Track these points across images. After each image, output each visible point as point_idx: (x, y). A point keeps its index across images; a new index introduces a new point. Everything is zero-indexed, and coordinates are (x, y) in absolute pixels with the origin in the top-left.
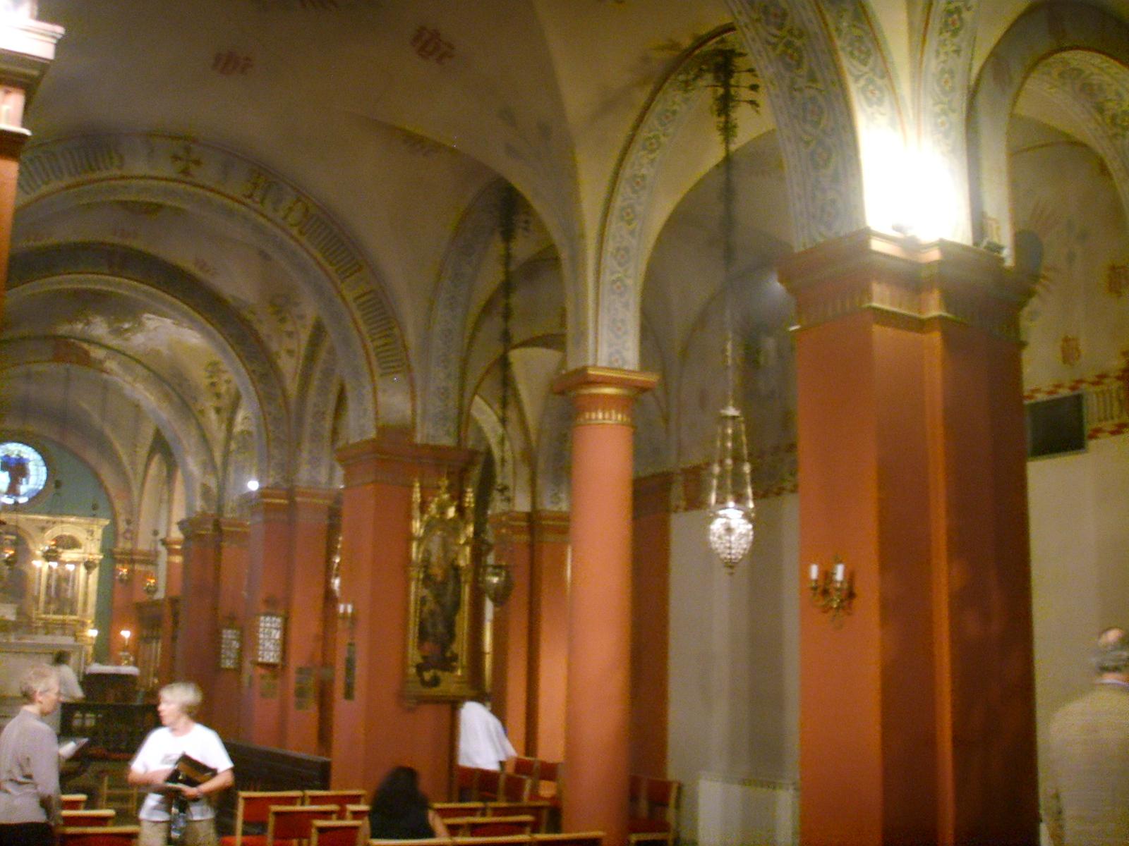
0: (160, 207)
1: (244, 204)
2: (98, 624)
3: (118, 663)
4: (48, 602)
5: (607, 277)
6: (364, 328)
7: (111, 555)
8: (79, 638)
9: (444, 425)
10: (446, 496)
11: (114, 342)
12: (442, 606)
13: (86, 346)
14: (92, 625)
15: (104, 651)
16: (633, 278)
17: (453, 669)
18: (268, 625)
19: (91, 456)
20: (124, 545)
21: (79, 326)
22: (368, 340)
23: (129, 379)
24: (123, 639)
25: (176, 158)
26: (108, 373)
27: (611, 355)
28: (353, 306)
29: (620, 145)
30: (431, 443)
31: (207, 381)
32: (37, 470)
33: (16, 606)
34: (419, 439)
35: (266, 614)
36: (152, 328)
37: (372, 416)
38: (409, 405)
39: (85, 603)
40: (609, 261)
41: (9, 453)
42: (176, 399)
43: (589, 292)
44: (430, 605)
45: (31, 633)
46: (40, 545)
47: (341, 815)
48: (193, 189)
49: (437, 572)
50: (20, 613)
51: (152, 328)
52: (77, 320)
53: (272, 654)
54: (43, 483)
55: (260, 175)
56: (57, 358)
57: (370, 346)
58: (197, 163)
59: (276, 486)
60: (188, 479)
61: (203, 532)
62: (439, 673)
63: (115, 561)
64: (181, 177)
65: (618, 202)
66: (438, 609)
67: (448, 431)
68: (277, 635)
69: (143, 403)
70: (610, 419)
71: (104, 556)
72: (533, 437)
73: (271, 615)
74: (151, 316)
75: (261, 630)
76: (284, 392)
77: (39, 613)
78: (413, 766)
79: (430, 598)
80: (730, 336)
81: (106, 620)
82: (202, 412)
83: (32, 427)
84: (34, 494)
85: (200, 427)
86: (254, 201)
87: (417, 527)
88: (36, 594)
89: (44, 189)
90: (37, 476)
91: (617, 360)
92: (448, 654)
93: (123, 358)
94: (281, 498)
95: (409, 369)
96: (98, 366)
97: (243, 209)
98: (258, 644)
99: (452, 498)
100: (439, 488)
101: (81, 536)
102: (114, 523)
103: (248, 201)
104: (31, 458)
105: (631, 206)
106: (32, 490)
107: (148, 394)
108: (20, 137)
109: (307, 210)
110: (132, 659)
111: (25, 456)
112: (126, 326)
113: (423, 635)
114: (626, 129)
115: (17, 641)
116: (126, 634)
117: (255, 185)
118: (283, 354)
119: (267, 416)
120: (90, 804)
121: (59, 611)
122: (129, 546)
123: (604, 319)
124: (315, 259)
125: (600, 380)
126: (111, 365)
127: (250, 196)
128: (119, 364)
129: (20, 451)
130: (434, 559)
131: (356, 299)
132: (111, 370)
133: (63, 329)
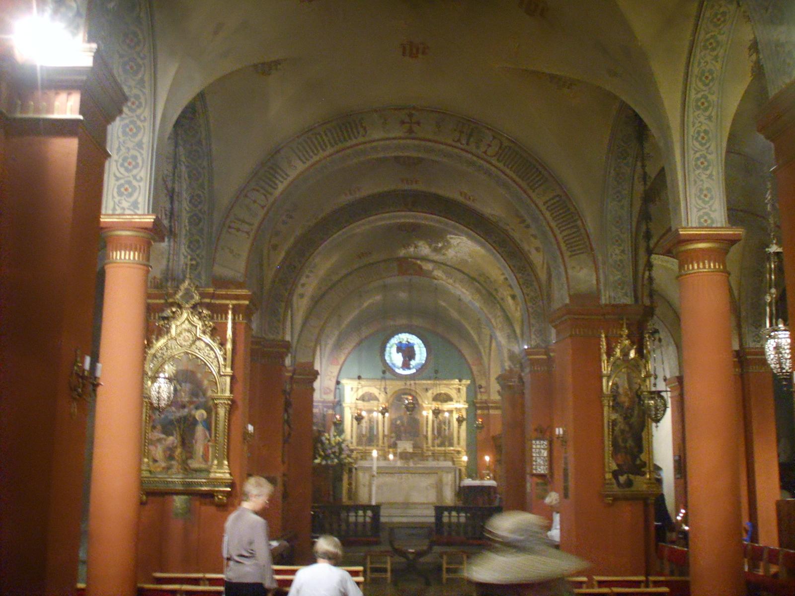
0: (421, 160)
1: (455, 147)
2: (469, 453)
3: (482, 478)
4: (434, 439)
5: (691, 156)
6: (553, 224)
7: (473, 405)
8: (456, 463)
9: (622, 289)
10: (627, 342)
11: (437, 257)
12: (631, 426)
13: (419, 262)
14: (465, 453)
15: (474, 470)
16: (716, 153)
17: (644, 474)
18: (538, 446)
19: (455, 339)
21: (412, 249)
22: (557, 232)
23: (451, 281)
24: (485, 461)
26: (436, 279)
27: (700, 217)
28: (543, 208)
29: (686, 51)
30: (613, 302)
31: (502, 278)
32: (420, 350)
33: (412, 442)
34: (603, 301)
35: (536, 439)
36: (455, 244)
37: (566, 287)
39: (459, 438)
40: (693, 144)
41: (401, 340)
42: (484, 292)
43: (678, 173)
44: (621, 425)
45: (423, 460)
47: (590, 584)
48: (464, 154)
49: (625, 400)
50: (415, 446)
51: (455, 244)
52: (409, 245)
53: (542, 467)
54: (425, 359)
56: (402, 272)
57: (560, 237)
58: (418, 123)
59: (537, 346)
60: (499, 345)
61: (511, 384)
62: (631, 477)
63: (477, 408)
65: (693, 96)
66: (627, 429)
68: (545, 453)
69: (462, 297)
70: (704, 268)
71: (469, 405)
72: (736, 293)
73: (540, 439)
74: (452, 236)
75: (534, 450)
76: (538, 280)
77: (430, 445)
79: (620, 419)
80: (769, 186)
81: (474, 449)
84: (420, 367)
85: (503, 310)
86: (462, 144)
87: (606, 369)
88: (425, 433)
89: (316, 158)
90: (421, 354)
91: (706, 221)
92: (638, 462)
93: (445, 267)
94: (541, 354)
96: (428, 275)
97: (456, 150)
98: (532, 461)
99: (633, 343)
100: (621, 336)
101: (453, 393)
102: (474, 381)
103: (459, 145)
104: (415, 343)
105: (706, 98)
106: (419, 364)
107: (464, 290)
108: (78, 121)
109: (501, 144)
110: (491, 475)
111: (411, 341)
112: (440, 245)
114: (688, 36)
115: (414, 466)
116: (487, 458)
118: (533, 251)
119: (526, 297)
121: (442, 444)
122: (485, 397)
123: (692, 191)
124: (511, 178)
125: (688, 238)
126: (438, 273)
127: (459, 141)
128: (443, 271)
129: (407, 339)
130: (621, 390)
132: (439, 277)
133: (402, 253)
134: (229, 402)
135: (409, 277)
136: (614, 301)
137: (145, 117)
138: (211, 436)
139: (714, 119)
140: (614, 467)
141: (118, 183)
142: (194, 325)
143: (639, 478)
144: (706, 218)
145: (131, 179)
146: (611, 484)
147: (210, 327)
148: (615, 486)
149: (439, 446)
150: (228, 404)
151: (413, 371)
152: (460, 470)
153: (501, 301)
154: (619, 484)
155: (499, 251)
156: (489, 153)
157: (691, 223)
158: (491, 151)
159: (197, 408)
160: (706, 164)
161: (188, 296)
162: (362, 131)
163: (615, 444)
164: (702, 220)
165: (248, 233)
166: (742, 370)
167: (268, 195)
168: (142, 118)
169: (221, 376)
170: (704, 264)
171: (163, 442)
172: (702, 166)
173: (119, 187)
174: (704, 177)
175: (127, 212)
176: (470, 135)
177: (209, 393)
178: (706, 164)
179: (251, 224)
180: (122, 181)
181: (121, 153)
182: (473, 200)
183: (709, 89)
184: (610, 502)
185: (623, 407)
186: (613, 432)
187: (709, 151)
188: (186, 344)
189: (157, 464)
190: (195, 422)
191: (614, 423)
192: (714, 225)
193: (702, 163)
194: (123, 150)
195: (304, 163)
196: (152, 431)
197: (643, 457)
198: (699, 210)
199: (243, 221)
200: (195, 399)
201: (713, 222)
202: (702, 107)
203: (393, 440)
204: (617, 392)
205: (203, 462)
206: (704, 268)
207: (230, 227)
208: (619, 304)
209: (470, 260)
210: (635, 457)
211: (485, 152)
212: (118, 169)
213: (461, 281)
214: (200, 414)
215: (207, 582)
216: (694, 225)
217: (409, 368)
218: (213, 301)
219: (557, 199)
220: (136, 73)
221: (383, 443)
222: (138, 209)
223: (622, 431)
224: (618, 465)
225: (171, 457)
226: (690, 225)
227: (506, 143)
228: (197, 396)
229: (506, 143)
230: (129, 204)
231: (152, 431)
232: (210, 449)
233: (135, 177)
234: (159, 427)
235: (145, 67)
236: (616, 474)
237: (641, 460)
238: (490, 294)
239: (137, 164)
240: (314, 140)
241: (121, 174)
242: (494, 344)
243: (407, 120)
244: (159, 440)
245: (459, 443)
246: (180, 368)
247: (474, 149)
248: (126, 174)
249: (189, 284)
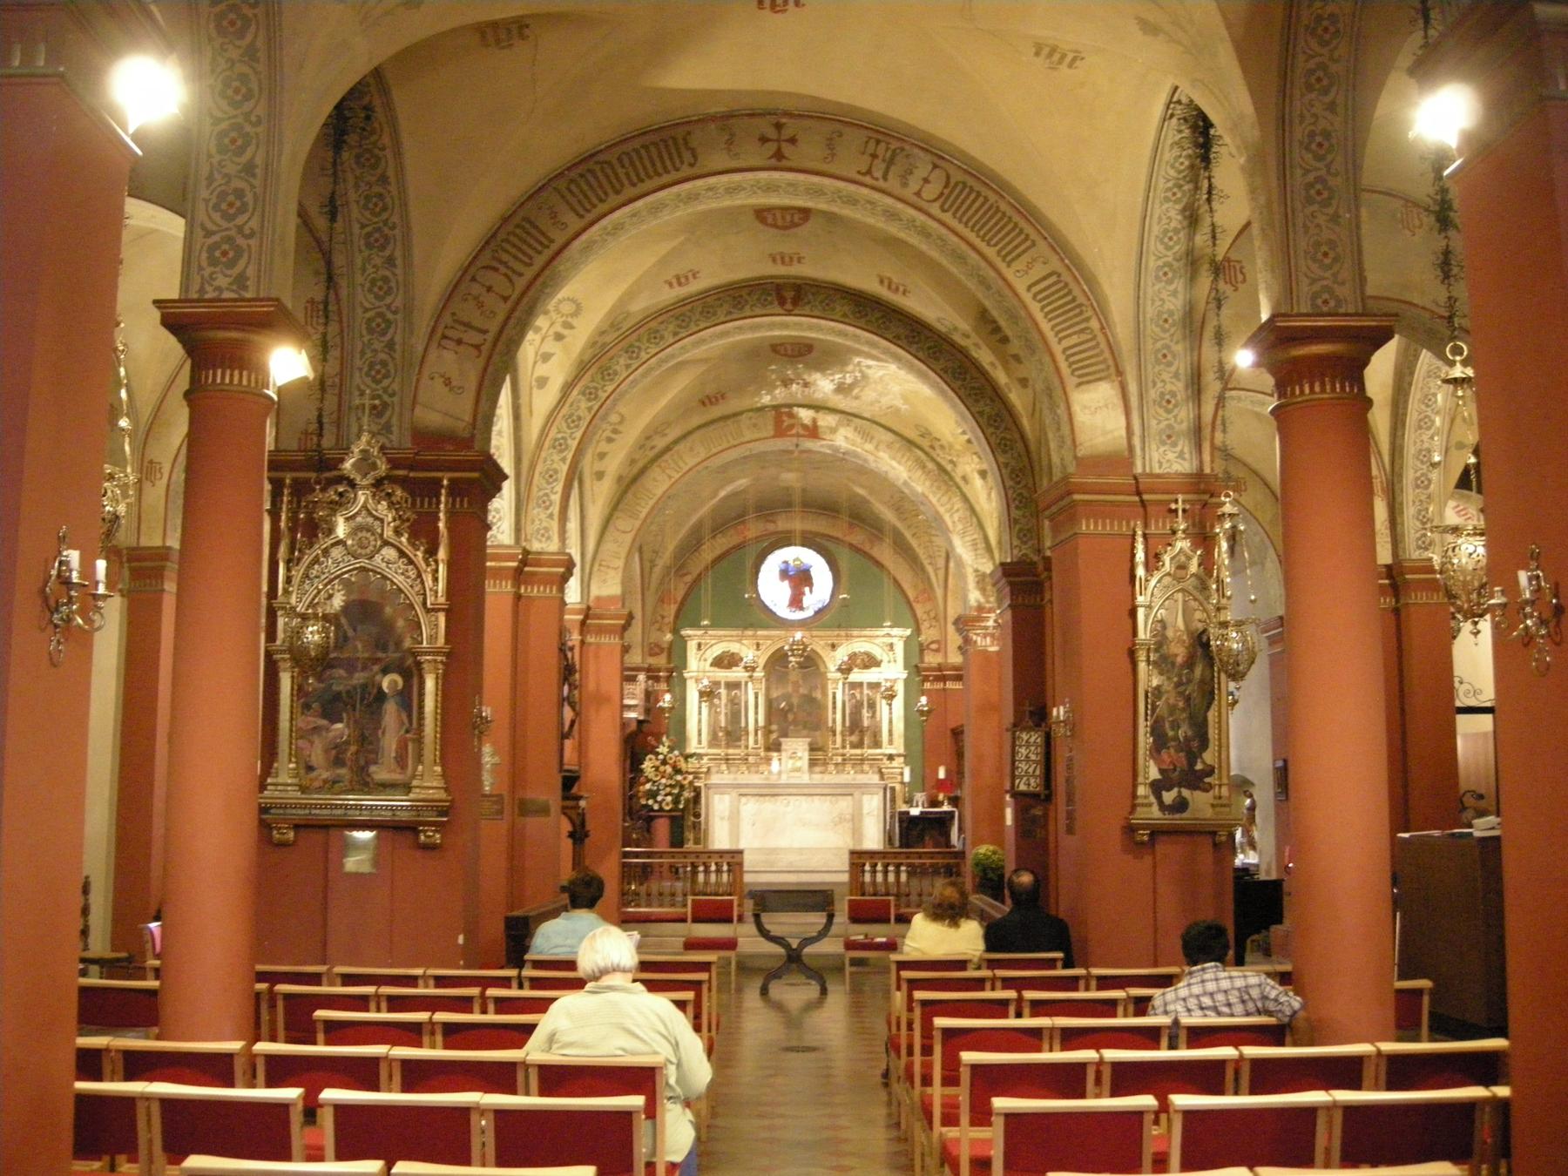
0: (805, 213)
20: (932, 659)
23: (869, 447)
25: (764, 140)
27: (1314, 297)
33: (808, 740)
38: (1122, 422)
48: (876, 196)
55: (878, 142)
58: (793, 141)
62: (1186, 793)
64: (773, 162)
67: (1182, 452)
78: (1070, 924)
79: (1168, 687)
86: (873, 178)
92: (1199, 766)
97: (865, 191)
99: (1195, 546)
101: (878, 652)
103: (867, 180)
109: (948, 177)
113: (1160, 742)
120: (1068, 964)
127: (869, 172)
130: (1170, 633)
131: (1029, 288)
134: (444, 659)
135: (795, 440)
136: (1160, 467)
137: (258, 116)
139: (1340, 109)
140: (1154, 773)
141: (210, 241)
142: (377, 518)
143: (1198, 794)
144: (1326, 296)
146: (1150, 805)
147: (408, 520)
148: (1155, 808)
149: (854, 746)
150: (442, 662)
151: (809, 613)
152: (893, 789)
153: (961, 483)
154: (1163, 807)
155: (953, 385)
156: (924, 195)
157: (1298, 305)
158: (931, 191)
159: (385, 672)
160: (1326, 194)
161: (365, 463)
162: (687, 156)
163: (1157, 731)
164: (1319, 301)
165: (477, 347)
166: (1397, 602)
167: (514, 278)
168: (253, 119)
169: (428, 611)
170: (1323, 385)
171: (324, 733)
172: (1319, 198)
173: (212, 249)
174: (1321, 219)
175: (226, 295)
176: (890, 162)
177: (407, 643)
178: (1326, 194)
180: (216, 238)
181: (215, 184)
182: (904, 293)
183: (1331, 51)
184: (1146, 838)
185: (1173, 664)
186: (1153, 710)
187: (1333, 171)
188: (363, 552)
189: (314, 774)
190: (381, 696)
192: (1342, 310)
193: (1319, 193)
195: (582, 217)
196: (303, 713)
197: (1209, 757)
198: (1313, 281)
199: (468, 325)
200: (380, 655)
201: (1339, 302)
202: (1317, 86)
203: (774, 736)
204: (1164, 637)
205: (398, 770)
206: (1323, 390)
207: (444, 337)
208: (1168, 473)
209: (904, 407)
210: (1192, 757)
211: (918, 194)
212: (210, 217)
216: (1303, 310)
217: (801, 608)
218: (412, 475)
219: (1054, 279)
220: (241, 34)
221: (756, 742)
222: (245, 288)
223: (1172, 709)
224: (1161, 771)
226: (1295, 311)
227: (957, 176)
228: (385, 649)
229: (957, 176)
230: (229, 280)
231: (303, 713)
232: (410, 746)
235: (258, 24)
237: (1204, 762)
240: (599, 174)
241: (215, 223)
242: (952, 565)
243: (771, 133)
244: (316, 730)
245: (891, 742)
246: (353, 597)
247: (898, 190)
248: (225, 224)
249: (369, 443)
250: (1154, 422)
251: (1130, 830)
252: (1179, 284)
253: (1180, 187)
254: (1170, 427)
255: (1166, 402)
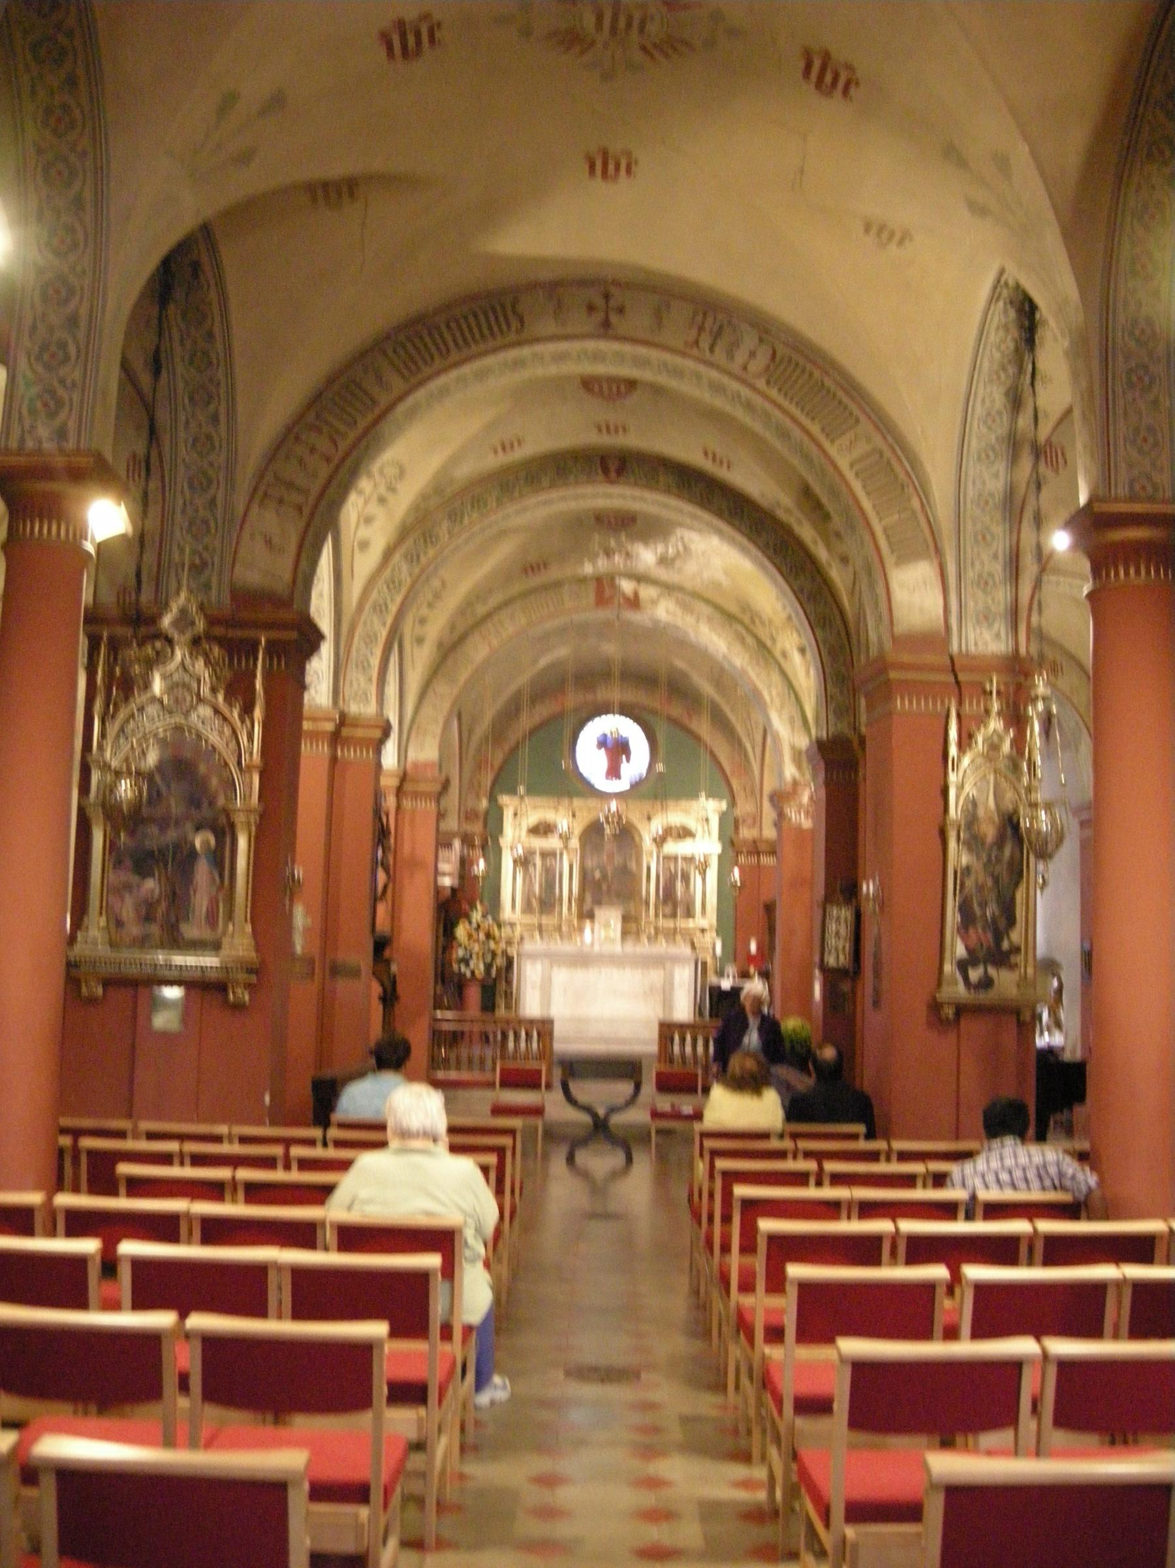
0: (632, 384)
44: (980, 875)
46: (220, 821)
58: (621, 310)
62: (992, 971)
66: (990, 883)
79: (978, 867)
82: (784, 654)
83: (603, 694)
95: (938, 551)
103: (695, 351)
117: (701, 329)
130: (981, 812)
138: (222, 881)
140: (960, 950)
145: (56, 383)
153: (782, 660)
159: (198, 828)
161: (183, 620)
162: (514, 323)
163: (965, 909)
179: (305, 492)
185: (983, 844)
190: (193, 854)
191: (967, 870)
194: (193, 425)
197: (1016, 936)
210: (998, 937)
212: (30, 364)
213: (710, 619)
214: (201, 840)
215: (727, 1258)
223: (980, 888)
225: (148, 918)
227: (781, 351)
233: (62, 382)
234: (128, 862)
236: (963, 966)
238: (761, 644)
239: (67, 359)
243: (599, 302)
250: (971, 604)
251: (935, 1007)
252: (1001, 466)
253: (1004, 369)
254: (987, 608)
255: (984, 583)
